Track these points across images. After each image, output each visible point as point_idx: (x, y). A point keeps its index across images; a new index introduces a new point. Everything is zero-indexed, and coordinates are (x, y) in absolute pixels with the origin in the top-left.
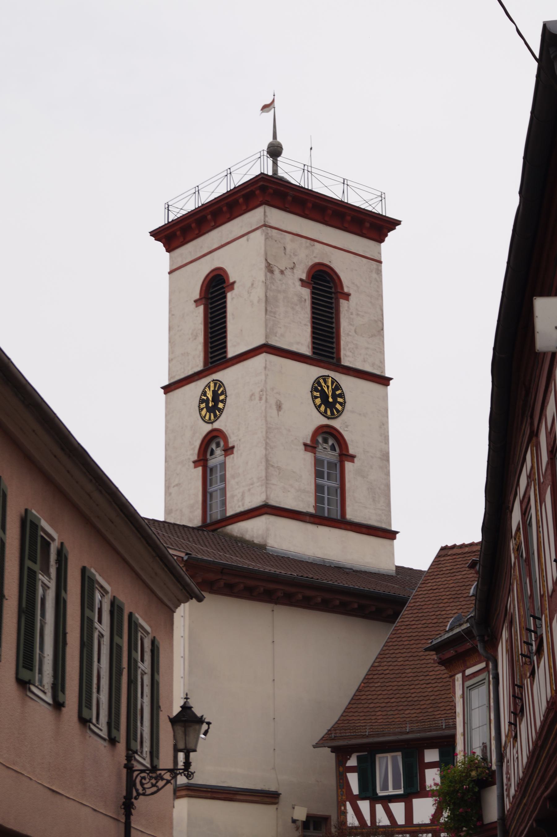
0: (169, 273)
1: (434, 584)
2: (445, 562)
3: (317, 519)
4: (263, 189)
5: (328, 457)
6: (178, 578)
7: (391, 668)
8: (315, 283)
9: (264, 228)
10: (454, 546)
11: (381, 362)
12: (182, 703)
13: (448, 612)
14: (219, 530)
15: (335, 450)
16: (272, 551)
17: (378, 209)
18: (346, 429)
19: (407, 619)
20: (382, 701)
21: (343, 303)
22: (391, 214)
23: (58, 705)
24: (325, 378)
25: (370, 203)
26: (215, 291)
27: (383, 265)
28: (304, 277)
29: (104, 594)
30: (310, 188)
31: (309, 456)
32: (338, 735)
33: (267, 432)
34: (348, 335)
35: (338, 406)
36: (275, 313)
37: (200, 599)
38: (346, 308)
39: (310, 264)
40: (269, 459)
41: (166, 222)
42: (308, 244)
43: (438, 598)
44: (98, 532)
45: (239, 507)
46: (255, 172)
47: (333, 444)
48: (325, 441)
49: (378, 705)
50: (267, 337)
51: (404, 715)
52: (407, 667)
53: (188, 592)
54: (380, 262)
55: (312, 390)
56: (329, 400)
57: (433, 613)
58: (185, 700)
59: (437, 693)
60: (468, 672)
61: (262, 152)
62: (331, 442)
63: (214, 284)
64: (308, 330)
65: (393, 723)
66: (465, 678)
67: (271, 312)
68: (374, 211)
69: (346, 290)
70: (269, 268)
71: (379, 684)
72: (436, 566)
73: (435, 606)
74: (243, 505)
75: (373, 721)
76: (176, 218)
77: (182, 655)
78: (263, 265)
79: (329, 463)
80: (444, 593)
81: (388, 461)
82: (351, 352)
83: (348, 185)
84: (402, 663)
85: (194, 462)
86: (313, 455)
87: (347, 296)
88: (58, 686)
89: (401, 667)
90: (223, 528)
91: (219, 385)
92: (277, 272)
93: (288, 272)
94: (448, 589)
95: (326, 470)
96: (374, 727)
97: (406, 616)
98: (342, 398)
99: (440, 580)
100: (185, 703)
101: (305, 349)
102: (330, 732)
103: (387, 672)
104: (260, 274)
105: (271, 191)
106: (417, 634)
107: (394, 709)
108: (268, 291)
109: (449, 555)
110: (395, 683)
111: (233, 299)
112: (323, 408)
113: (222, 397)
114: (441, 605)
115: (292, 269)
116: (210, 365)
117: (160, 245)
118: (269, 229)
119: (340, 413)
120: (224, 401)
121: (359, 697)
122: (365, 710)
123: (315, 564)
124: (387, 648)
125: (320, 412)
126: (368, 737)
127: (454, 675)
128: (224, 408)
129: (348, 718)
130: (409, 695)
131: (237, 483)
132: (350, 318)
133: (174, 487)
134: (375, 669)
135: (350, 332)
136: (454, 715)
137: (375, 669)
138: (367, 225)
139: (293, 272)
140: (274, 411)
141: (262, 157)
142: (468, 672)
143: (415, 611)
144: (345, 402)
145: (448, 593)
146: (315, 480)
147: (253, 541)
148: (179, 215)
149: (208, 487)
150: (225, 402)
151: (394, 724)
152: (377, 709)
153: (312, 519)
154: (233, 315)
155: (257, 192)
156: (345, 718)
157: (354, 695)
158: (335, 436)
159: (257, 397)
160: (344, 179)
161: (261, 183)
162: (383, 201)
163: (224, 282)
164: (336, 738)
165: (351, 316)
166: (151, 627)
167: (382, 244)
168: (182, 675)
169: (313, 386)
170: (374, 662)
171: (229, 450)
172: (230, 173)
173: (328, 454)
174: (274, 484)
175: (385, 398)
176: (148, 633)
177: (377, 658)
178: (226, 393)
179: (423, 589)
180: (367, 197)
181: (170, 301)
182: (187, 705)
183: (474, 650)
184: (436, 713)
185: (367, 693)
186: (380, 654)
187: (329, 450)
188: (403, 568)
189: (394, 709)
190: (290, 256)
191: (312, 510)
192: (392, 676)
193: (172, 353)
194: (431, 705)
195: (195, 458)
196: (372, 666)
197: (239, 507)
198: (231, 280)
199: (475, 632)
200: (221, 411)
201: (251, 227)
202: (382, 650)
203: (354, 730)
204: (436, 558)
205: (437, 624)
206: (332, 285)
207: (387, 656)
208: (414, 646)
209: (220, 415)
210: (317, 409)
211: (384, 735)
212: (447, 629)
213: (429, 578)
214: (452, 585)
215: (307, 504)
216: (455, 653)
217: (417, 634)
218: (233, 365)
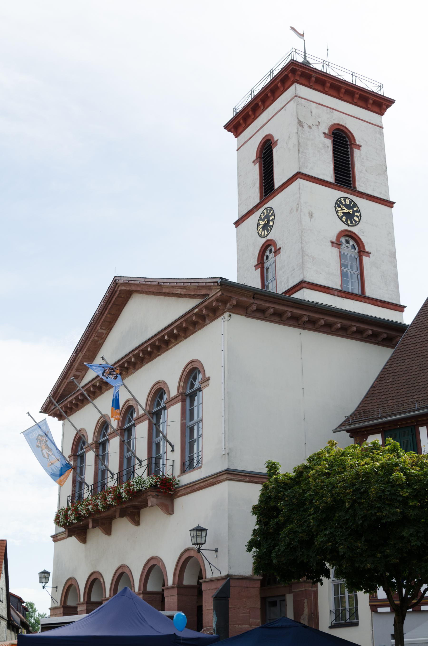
4: (294, 71)
7: (400, 367)
11: (386, 192)
15: (355, 249)
18: (362, 234)
19: (412, 332)
21: (356, 151)
22: (387, 93)
24: (345, 198)
26: (266, 154)
27: (384, 130)
28: (326, 131)
31: (335, 251)
34: (361, 172)
36: (305, 153)
38: (359, 155)
39: (331, 124)
40: (305, 250)
47: (353, 245)
48: (347, 242)
49: (389, 395)
56: (350, 215)
62: (352, 242)
67: (302, 152)
69: (358, 143)
70: (300, 124)
71: (390, 380)
77: (223, 365)
78: (296, 122)
81: (395, 258)
83: (355, 76)
84: (409, 363)
87: (359, 147)
92: (306, 127)
93: (314, 128)
103: (397, 370)
104: (294, 128)
105: (300, 73)
110: (404, 378)
111: (277, 152)
112: (344, 219)
115: (318, 126)
116: (264, 198)
119: (357, 223)
120: (273, 220)
121: (373, 392)
122: (378, 401)
124: (396, 354)
125: (342, 221)
129: (363, 408)
130: (416, 384)
131: (284, 272)
140: (307, 218)
144: (361, 216)
146: (341, 268)
153: (339, 294)
154: (277, 161)
155: (290, 75)
159: (295, 210)
161: (292, 67)
162: (382, 89)
168: (223, 381)
172: (273, 72)
173: (349, 250)
175: (391, 215)
181: (238, 168)
187: (351, 248)
190: (316, 117)
191: (339, 288)
195: (256, 263)
198: (275, 140)
200: (272, 227)
202: (392, 356)
206: (347, 140)
207: (396, 360)
208: (419, 349)
210: (340, 219)
218: (278, 194)
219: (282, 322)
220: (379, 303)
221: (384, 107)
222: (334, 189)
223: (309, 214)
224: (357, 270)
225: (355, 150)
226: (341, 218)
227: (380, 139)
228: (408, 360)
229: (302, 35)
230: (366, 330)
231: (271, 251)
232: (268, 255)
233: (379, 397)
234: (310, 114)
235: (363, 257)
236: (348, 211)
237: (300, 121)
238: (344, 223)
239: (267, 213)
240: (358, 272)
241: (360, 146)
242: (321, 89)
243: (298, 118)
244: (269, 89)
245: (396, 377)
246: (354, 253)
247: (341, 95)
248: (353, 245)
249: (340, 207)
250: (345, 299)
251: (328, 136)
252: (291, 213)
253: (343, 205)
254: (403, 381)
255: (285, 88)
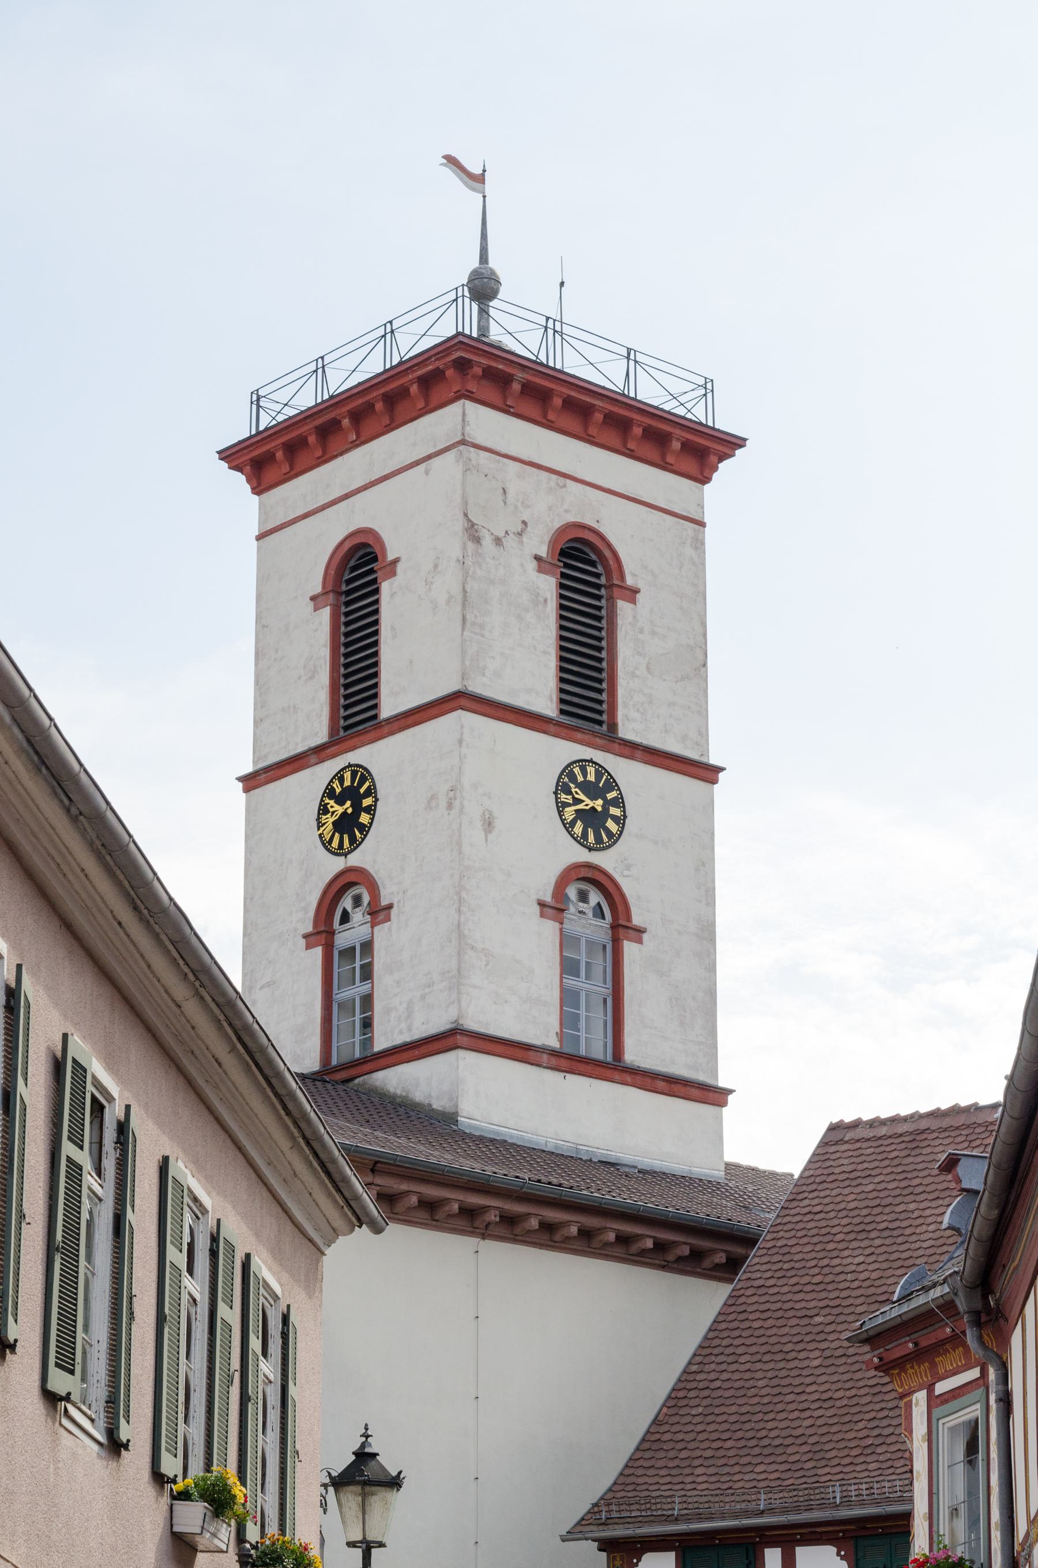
0: (259, 538)
1: (816, 1201)
2: (838, 1155)
3: (568, 1061)
4: (462, 366)
5: (588, 932)
6: (337, 1184)
7: (725, 1376)
8: (567, 566)
9: (462, 448)
10: (856, 1124)
11: (700, 733)
12: (356, 1446)
13: (845, 1262)
14: (357, 1081)
15: (603, 918)
16: (470, 1126)
17: (699, 414)
18: (626, 873)
20: (706, 1444)
22: (725, 423)
23: (115, 1446)
25: (682, 399)
26: (357, 575)
28: (543, 552)
29: (200, 1215)
30: (558, 366)
31: (550, 929)
32: (615, 1515)
33: (462, 877)
34: (633, 675)
35: (611, 825)
36: (482, 626)
37: (377, 1230)
38: (630, 619)
39: (557, 524)
40: (466, 932)
41: (254, 432)
42: (553, 484)
43: (823, 1231)
44: (190, 1083)
45: (401, 1032)
46: (446, 330)
47: (599, 904)
48: (583, 897)
49: (698, 1453)
50: (464, 676)
51: (752, 1476)
52: (759, 1375)
53: (354, 1213)
54: (702, 524)
55: (557, 789)
56: (593, 810)
57: (813, 1263)
58: (364, 1439)
59: (824, 1430)
60: (942, 1387)
61: (460, 290)
62: (595, 897)
63: (352, 563)
64: (551, 663)
65: (730, 1491)
66: (933, 1402)
67: (473, 624)
68: (689, 416)
69: (630, 581)
70: (472, 533)
71: (700, 1409)
72: (818, 1164)
73: (818, 1247)
74: (410, 1029)
75: (689, 1487)
76: (274, 422)
78: (460, 524)
79: (590, 943)
80: (836, 1222)
81: (713, 940)
82: (638, 710)
83: (636, 362)
84: (748, 1366)
85: (306, 936)
86: (557, 925)
87: (632, 594)
88: (115, 1405)
89: (747, 1376)
90: (366, 1077)
91: (362, 774)
92: (487, 541)
93: (510, 542)
94: (844, 1213)
95: (583, 959)
96: (690, 1500)
97: (757, 1267)
98: (619, 807)
99: (828, 1192)
100: (363, 1445)
101: (547, 705)
102: (596, 1509)
103: (718, 1384)
104: (453, 544)
105: (478, 371)
106: (779, 1305)
107: (732, 1462)
108: (469, 579)
109: (847, 1142)
110: (734, 1409)
111: (392, 595)
113: (367, 802)
114: (831, 1246)
115: (520, 534)
117: (239, 478)
118: (472, 449)
119: (614, 839)
120: (371, 810)
123: (558, 1155)
124: (716, 1333)
125: (572, 836)
126: (677, 1520)
127: (911, 1393)
128: (371, 824)
130: (763, 1433)
131: (398, 982)
132: (637, 639)
133: (262, 988)
134: (691, 1377)
135: (636, 668)
136: (908, 1475)
137: (691, 1377)
138: (676, 445)
139: (521, 542)
140: (474, 834)
141: (460, 300)
142: (942, 1387)
143: (776, 1258)
144: (625, 817)
145: (845, 1221)
146: (561, 978)
147: (430, 1105)
148: (280, 418)
149: (335, 990)
150: (375, 810)
151: (733, 1494)
152: (696, 1462)
153: (554, 1061)
154: (393, 628)
155: (450, 373)
156: (629, 1480)
157: (648, 1432)
158: (603, 885)
159: (443, 804)
160: (629, 350)
161: (459, 354)
162: (709, 395)
163: (375, 559)
164: (609, 1521)
165: (641, 636)
166: (281, 1285)
167: (707, 487)
169: (558, 781)
170: (690, 1363)
171: (379, 913)
172: (392, 332)
173: (588, 924)
174: (474, 987)
176: (276, 1298)
177: (695, 1355)
178: (376, 792)
179: (792, 1212)
180: (676, 386)
182: (367, 1450)
183: (957, 1340)
184: (820, 1472)
185: (675, 1429)
186: (701, 1347)
187: (590, 914)
188: (737, 1166)
189: (732, 1462)
190: (516, 507)
191: (554, 1043)
192: (727, 1394)
193: (262, 707)
194: (810, 1455)
195: (309, 928)
196: (685, 1372)
197: (401, 1032)
198: (390, 557)
199: (961, 1304)
200: (365, 829)
201: (435, 445)
203: (648, 1506)
204: (818, 1147)
205: (822, 1287)
206: (600, 569)
207: (716, 1351)
208: (774, 1331)
209: (363, 840)
211: (711, 1519)
212: (895, 1299)
213: (804, 1188)
214: (852, 1205)
215: (544, 1032)
216: (909, 1347)
217: (779, 1305)
218: (392, 733)
219: (434, 1223)
220: (661, 1084)
221: (713, 459)
222: (556, 735)
223: (485, 820)
224: (605, 983)
225: (621, 604)
226: (569, 827)
227: (694, 564)
228: (747, 1358)
229: (477, 180)
230: (638, 1237)
231: (357, 901)
232: (349, 909)
233: (672, 1454)
234: (501, 498)
235: (625, 942)
236: (591, 804)
237: (473, 525)
238: (579, 842)
239: (353, 780)
240: (606, 990)
241: (635, 591)
242: (535, 414)
243: (466, 515)
244: (382, 391)
245: (716, 1402)
246: (597, 930)
247: (593, 431)
248: (599, 904)
249: (570, 793)
250: (568, 1076)
251: (547, 566)
252: (429, 807)
253: (579, 785)
254: (733, 1419)
255: (431, 406)
